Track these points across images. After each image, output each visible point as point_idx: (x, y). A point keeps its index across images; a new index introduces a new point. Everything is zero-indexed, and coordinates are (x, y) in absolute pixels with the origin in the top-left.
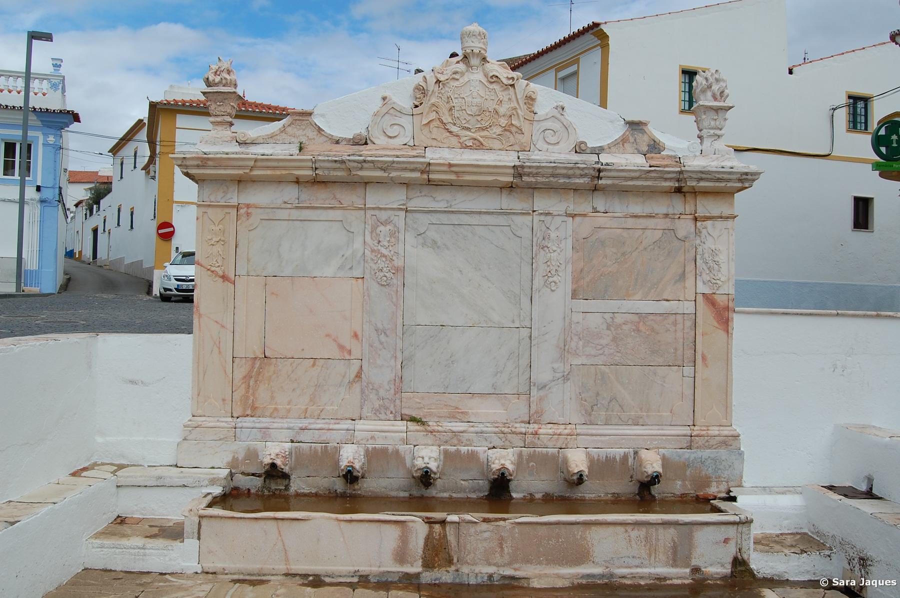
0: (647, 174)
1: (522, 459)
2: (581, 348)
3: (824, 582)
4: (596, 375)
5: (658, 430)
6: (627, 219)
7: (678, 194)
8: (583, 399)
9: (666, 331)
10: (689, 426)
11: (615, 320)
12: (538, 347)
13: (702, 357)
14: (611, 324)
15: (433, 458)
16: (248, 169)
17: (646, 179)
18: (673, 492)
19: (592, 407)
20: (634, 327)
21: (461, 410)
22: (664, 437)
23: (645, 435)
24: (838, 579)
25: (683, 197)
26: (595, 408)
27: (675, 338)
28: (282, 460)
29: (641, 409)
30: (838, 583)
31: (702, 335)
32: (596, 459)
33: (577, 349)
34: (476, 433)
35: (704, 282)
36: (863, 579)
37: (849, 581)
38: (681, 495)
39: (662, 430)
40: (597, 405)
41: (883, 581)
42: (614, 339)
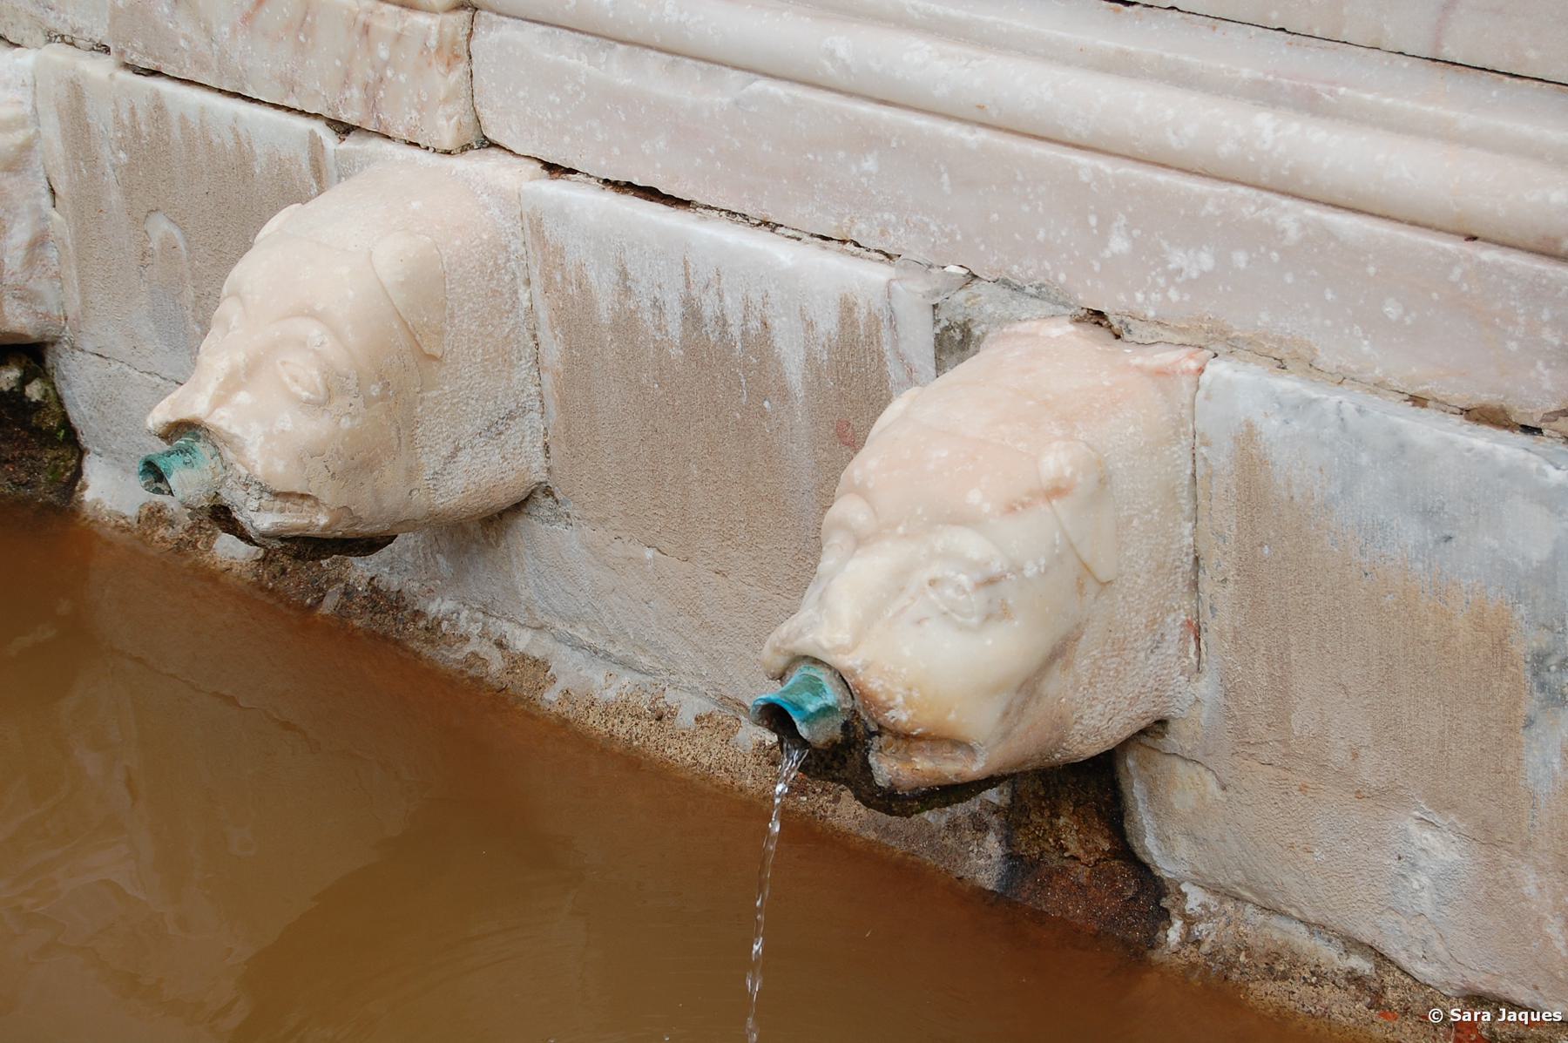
3: (1436, 1016)
5: (1265, 95)
18: (1366, 933)
22: (1291, 217)
23: (1078, 129)
24: (1459, 1010)
30: (1459, 1016)
37: (1479, 1013)
39: (1310, 104)
41: (1538, 1013)
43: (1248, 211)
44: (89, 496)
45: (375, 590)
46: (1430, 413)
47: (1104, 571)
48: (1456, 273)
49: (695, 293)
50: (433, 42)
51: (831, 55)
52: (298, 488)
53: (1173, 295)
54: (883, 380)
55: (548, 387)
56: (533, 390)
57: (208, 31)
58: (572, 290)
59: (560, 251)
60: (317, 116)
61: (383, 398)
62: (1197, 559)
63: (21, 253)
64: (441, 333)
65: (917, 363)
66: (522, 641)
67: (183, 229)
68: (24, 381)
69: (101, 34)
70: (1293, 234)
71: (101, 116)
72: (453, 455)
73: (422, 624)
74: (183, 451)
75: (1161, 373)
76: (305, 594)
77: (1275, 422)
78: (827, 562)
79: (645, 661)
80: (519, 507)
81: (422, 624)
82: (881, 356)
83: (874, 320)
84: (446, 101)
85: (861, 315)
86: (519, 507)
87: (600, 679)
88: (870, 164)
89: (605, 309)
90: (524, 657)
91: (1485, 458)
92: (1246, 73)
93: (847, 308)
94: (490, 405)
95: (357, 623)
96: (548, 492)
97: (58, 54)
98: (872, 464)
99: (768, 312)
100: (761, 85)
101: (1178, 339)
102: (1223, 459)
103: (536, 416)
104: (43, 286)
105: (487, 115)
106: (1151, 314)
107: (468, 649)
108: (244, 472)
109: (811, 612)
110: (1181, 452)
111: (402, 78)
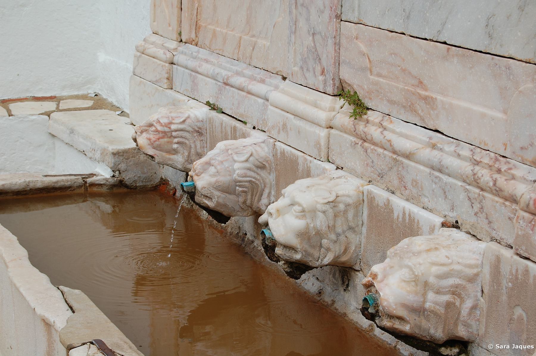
1: (499, 284)
15: (300, 205)
21: (426, 90)
24: (499, 345)
28: (151, 136)
34: (432, 168)
36: (514, 345)
38: (102, 109)
41: (526, 346)
63: (468, 310)
67: (527, 314)
69: (510, 241)
71: (505, 269)
97: (494, 246)
104: (473, 323)
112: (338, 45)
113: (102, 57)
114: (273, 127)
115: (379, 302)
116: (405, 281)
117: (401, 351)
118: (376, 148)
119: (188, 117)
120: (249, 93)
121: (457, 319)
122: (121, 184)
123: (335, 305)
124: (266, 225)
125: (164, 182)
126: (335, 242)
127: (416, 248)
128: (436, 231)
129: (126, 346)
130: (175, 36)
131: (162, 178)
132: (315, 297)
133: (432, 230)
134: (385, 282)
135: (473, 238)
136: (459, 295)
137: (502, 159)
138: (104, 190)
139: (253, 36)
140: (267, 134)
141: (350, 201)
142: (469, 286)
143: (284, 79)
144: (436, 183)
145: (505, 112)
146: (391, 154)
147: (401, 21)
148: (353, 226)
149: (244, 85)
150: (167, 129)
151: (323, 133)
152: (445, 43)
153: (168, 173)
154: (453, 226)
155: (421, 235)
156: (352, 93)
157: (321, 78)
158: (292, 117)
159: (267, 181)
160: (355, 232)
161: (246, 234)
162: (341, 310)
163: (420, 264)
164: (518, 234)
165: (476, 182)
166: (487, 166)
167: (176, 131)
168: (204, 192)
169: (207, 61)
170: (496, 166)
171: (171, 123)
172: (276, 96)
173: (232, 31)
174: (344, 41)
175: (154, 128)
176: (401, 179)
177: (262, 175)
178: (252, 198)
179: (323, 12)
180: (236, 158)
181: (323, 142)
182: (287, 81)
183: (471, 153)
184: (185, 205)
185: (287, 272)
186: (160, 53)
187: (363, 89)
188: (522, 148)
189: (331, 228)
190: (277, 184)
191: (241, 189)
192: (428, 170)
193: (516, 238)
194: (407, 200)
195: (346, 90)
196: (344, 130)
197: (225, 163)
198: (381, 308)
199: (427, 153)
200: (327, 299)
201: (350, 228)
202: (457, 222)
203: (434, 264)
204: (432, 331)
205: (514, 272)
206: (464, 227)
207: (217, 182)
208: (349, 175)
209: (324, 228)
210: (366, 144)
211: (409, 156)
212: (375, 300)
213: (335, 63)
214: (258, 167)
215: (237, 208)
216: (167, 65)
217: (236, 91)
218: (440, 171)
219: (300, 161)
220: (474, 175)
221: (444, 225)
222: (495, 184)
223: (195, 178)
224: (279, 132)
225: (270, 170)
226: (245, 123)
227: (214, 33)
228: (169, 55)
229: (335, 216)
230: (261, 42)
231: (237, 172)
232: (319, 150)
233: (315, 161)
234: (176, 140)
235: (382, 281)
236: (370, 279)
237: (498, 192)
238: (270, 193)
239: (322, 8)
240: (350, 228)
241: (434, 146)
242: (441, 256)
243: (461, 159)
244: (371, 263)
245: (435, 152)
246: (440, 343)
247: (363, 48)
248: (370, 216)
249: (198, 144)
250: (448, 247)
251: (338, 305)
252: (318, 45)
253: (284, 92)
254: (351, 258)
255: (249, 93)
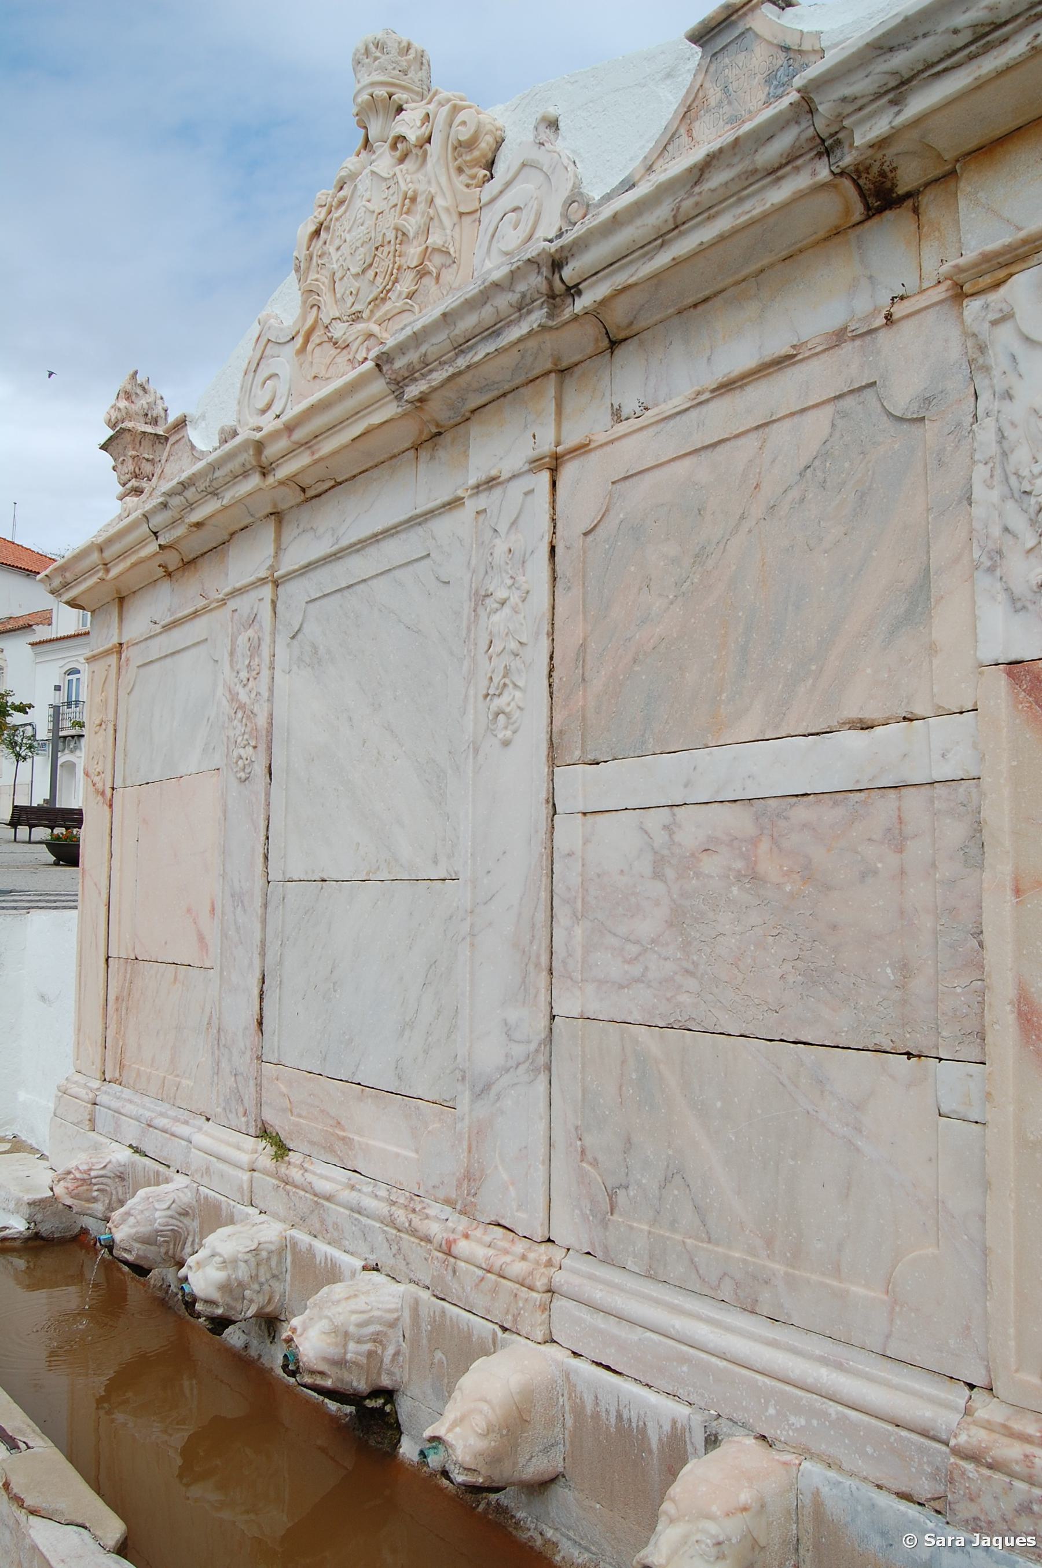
0: (697, 189)
1: (419, 1328)
2: (579, 952)
4: (623, 1062)
5: (824, 1361)
6: (704, 409)
7: (889, 215)
8: (589, 1156)
9: (863, 876)
10: (972, 1387)
11: (677, 838)
12: (472, 945)
13: (1020, 1014)
14: (666, 852)
15: (221, 1256)
16: (98, 571)
17: (707, 212)
19: (612, 1196)
20: (739, 865)
21: (344, 1131)
22: (834, 1409)
23: (758, 1366)
25: (911, 214)
26: (622, 1197)
27: (902, 913)
28: (69, 1185)
29: (769, 1242)
31: (1017, 892)
32: (589, 1413)
33: (570, 955)
34: (352, 1210)
35: (1013, 600)
39: (839, 1367)
40: (627, 1187)
42: (677, 919)
43: (818, 1405)
44: (401, 1451)
45: (498, 1504)
46: (884, 1493)
47: (762, 1542)
48: (892, 1439)
49: (621, 1408)
50: (538, 1303)
51: (673, 1327)
52: (473, 1467)
53: (791, 1433)
54: (686, 1451)
55: (566, 1436)
56: (561, 1436)
57: (463, 1288)
58: (578, 1400)
59: (575, 1386)
60: (496, 1323)
61: (507, 1435)
62: (798, 1540)
63: (390, 1357)
64: (530, 1412)
65: (698, 1447)
66: (549, 1533)
67: (446, 1357)
68: (385, 1404)
69: (427, 1283)
70: (834, 1416)
71: (424, 1312)
72: (530, 1459)
73: (514, 1521)
74: (434, 1448)
75: (785, 1463)
76: (473, 1502)
77: (827, 1489)
78: (659, 1528)
79: (593, 1548)
80: (553, 1480)
81: (514, 1521)
82: (685, 1442)
83: (683, 1428)
84: (540, 1325)
85: (679, 1426)
86: (553, 1480)
87: (576, 1554)
88: (685, 1368)
89: (589, 1408)
90: (549, 1540)
91: (904, 1514)
92: (817, 1352)
93: (674, 1422)
94: (545, 1440)
95: (490, 1517)
96: (564, 1476)
97: (412, 1287)
98: (678, 1490)
99: (646, 1419)
100: (649, 1334)
101: (793, 1450)
102: (808, 1501)
103: (562, 1446)
104: (396, 1370)
105: (554, 1331)
106: (783, 1439)
107: (530, 1534)
108: (455, 1459)
109: (652, 1548)
110: (792, 1495)
111: (526, 1314)
112: (259, 1086)
113: (22, 1096)
114: (196, 1171)
115: (299, 1357)
116: (325, 1333)
117: (329, 1406)
118: (297, 1191)
119: (110, 1162)
120: (173, 1135)
121: (380, 1368)
122: (37, 1236)
123: (262, 1360)
124: (186, 1279)
125: (84, 1231)
126: (259, 1292)
127: (336, 1297)
128: (357, 1275)
129: (29, 1430)
130: (99, 1075)
131: (82, 1227)
132: (241, 1352)
133: (353, 1274)
134: (304, 1336)
135: (393, 1281)
136: (381, 1342)
137: (416, 1198)
138: (17, 1244)
139: (177, 1076)
140: (191, 1178)
141: (273, 1247)
142: (390, 1331)
143: (208, 1119)
144: (355, 1225)
145: (417, 1151)
146: (312, 1197)
147: (319, 1063)
148: (277, 1273)
149: (167, 1127)
150: (86, 1176)
151: (245, 1176)
152: (359, 1084)
153: (89, 1223)
154: (374, 1269)
155: (340, 1281)
156: (274, 1134)
157: (244, 1119)
158: (215, 1160)
159: (191, 1228)
160: (279, 1279)
161: (170, 1286)
162: (268, 1365)
163: (339, 1314)
164: (433, 1275)
165: (392, 1223)
166: (403, 1206)
167: (96, 1178)
168: (124, 1245)
169: (130, 1101)
170: (411, 1205)
171: (90, 1170)
172: (199, 1138)
173: (157, 1070)
174: (265, 1082)
175: (72, 1176)
176: (322, 1222)
177: (185, 1222)
178: (174, 1248)
179: (244, 1053)
180: (157, 1206)
181: (246, 1186)
182: (210, 1122)
183: (387, 1193)
184: (106, 1256)
185: (208, 1329)
186: (82, 1092)
187: (285, 1130)
188: (434, 1187)
189: (254, 1278)
190: (201, 1232)
191: (162, 1239)
192: (347, 1212)
193: (432, 1279)
194: (329, 1244)
195: (268, 1131)
196: (265, 1172)
197: (145, 1212)
198: (301, 1364)
199: (346, 1195)
200: (253, 1353)
201: (274, 1276)
202: (377, 1265)
203: (353, 1312)
204: (355, 1384)
205: (432, 1314)
206: (385, 1269)
207: (137, 1233)
208: (272, 1219)
209: (246, 1279)
210: (288, 1187)
211: (329, 1198)
212: (296, 1356)
213: (257, 1104)
214: (180, 1214)
215: (159, 1259)
216: (89, 1106)
217: (160, 1132)
218: (359, 1213)
219: (224, 1206)
220: (391, 1215)
221: (364, 1268)
222: (410, 1225)
223: (114, 1230)
224: (202, 1176)
225: (194, 1216)
226: (169, 1166)
227: (138, 1072)
228: (91, 1095)
229: (258, 1264)
230: (185, 1082)
231: (158, 1221)
232: (243, 1196)
233: (239, 1205)
234: (96, 1187)
235: (301, 1335)
236: (290, 1333)
237: (413, 1232)
238: (193, 1241)
239: (243, 1049)
240: (274, 1276)
241: (353, 1188)
242: (360, 1303)
243: (379, 1200)
244: (296, 1312)
245: (354, 1194)
246: (364, 1395)
247: (283, 1088)
248: (293, 1261)
249: (120, 1190)
250: (368, 1292)
251: (264, 1360)
252: (240, 1086)
253: (207, 1134)
254: (275, 1308)
255: (173, 1135)
